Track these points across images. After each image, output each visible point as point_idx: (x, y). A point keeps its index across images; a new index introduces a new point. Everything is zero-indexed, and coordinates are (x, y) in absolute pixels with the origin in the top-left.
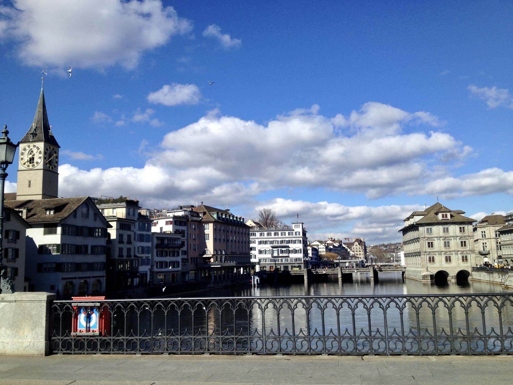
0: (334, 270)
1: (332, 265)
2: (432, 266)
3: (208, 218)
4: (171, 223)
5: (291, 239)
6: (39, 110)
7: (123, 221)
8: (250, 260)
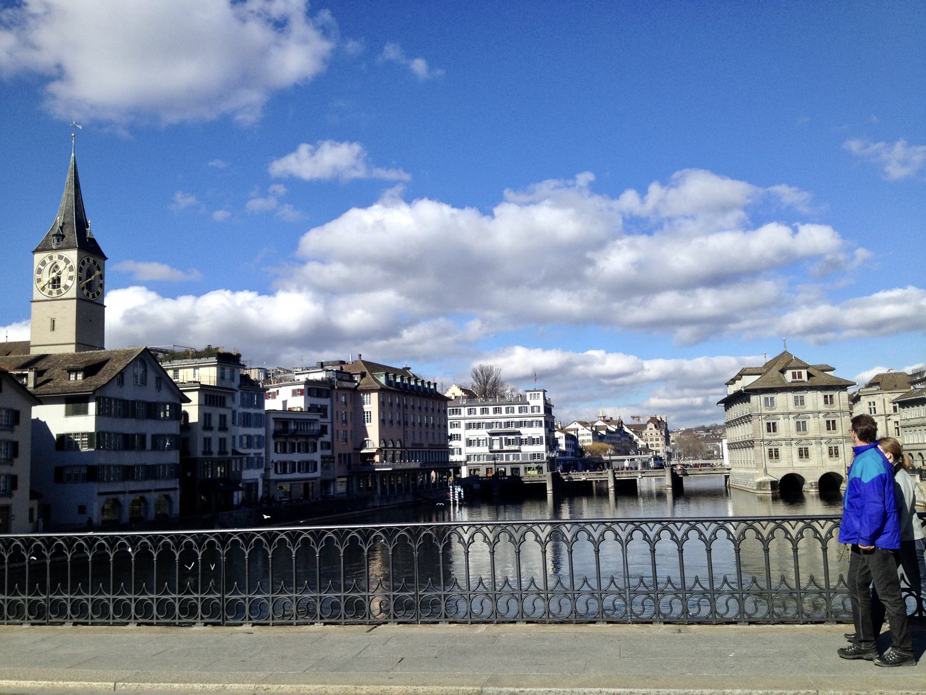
0: (601, 474)
1: (597, 464)
2: (775, 465)
3: (370, 384)
4: (302, 392)
5: (523, 419)
6: (68, 192)
7: (207, 390)
8: (448, 458)
